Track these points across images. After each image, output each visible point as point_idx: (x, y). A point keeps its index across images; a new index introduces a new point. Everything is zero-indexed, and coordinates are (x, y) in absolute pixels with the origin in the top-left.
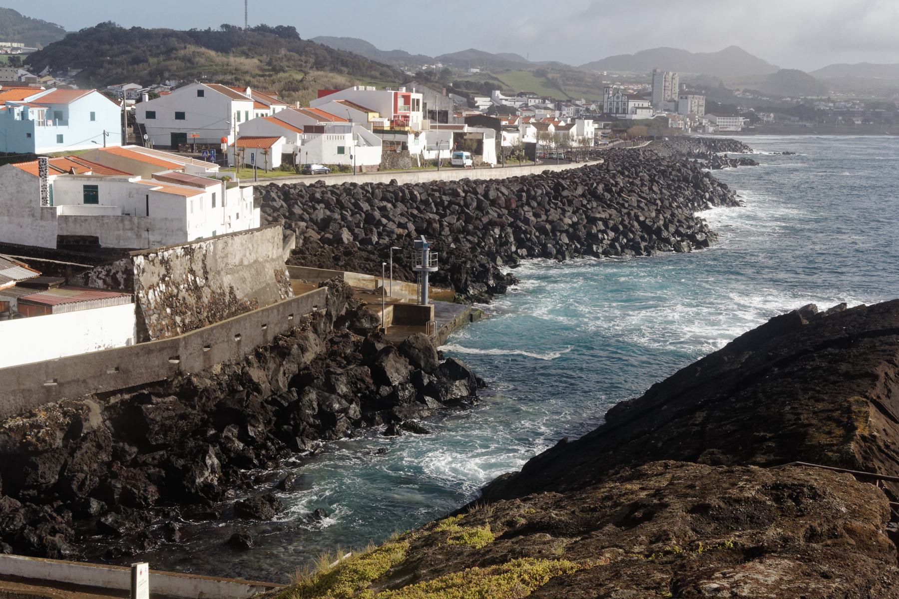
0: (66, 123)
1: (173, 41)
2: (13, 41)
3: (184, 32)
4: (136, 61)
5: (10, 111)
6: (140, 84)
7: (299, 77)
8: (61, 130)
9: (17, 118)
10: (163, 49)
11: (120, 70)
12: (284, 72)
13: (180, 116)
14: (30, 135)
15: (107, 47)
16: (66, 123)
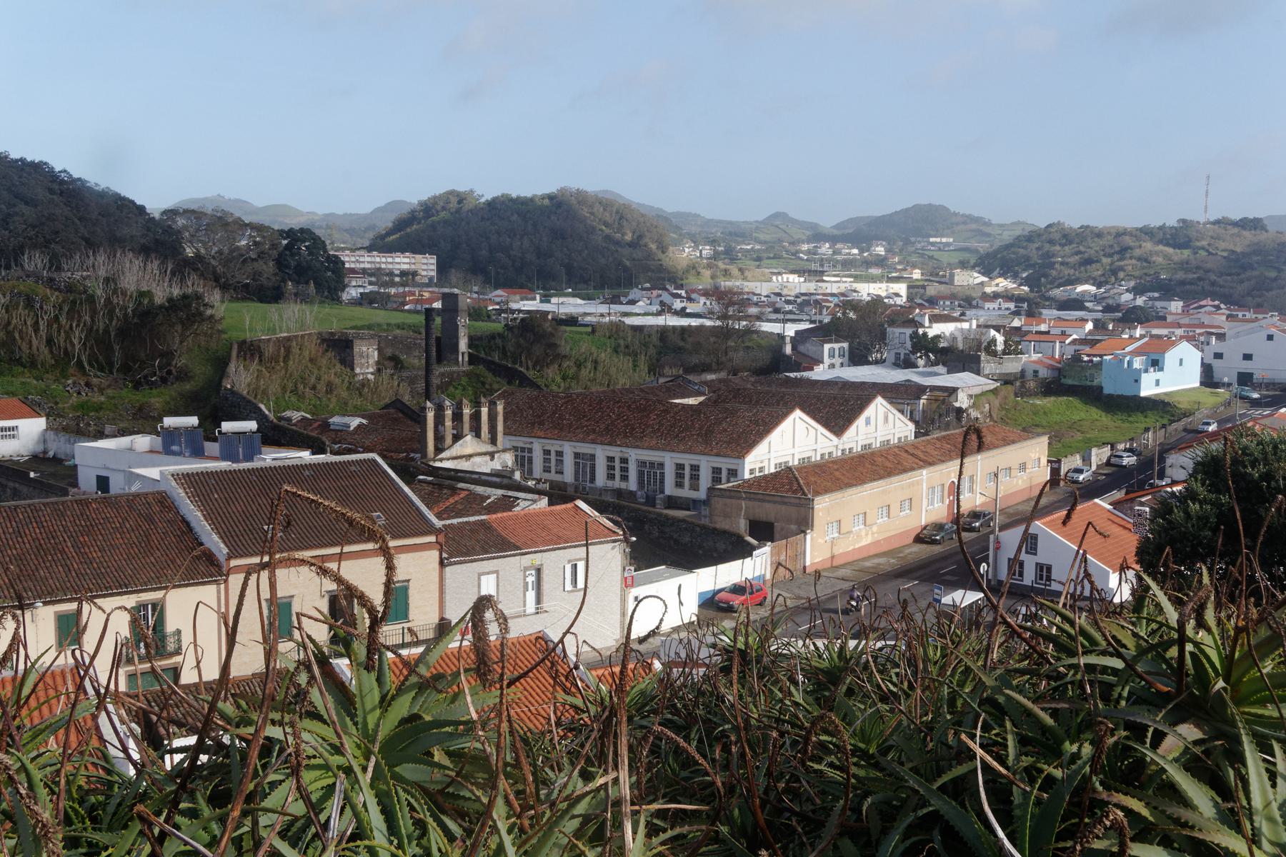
0: (1161, 369)
1: (1128, 240)
2: (942, 236)
3: (1137, 229)
4: (1089, 262)
5: (1122, 361)
7: (1273, 274)
8: (1159, 375)
10: (1117, 249)
12: (1253, 269)
13: (1248, 357)
14: (1137, 381)
15: (1058, 248)
16: (1161, 369)
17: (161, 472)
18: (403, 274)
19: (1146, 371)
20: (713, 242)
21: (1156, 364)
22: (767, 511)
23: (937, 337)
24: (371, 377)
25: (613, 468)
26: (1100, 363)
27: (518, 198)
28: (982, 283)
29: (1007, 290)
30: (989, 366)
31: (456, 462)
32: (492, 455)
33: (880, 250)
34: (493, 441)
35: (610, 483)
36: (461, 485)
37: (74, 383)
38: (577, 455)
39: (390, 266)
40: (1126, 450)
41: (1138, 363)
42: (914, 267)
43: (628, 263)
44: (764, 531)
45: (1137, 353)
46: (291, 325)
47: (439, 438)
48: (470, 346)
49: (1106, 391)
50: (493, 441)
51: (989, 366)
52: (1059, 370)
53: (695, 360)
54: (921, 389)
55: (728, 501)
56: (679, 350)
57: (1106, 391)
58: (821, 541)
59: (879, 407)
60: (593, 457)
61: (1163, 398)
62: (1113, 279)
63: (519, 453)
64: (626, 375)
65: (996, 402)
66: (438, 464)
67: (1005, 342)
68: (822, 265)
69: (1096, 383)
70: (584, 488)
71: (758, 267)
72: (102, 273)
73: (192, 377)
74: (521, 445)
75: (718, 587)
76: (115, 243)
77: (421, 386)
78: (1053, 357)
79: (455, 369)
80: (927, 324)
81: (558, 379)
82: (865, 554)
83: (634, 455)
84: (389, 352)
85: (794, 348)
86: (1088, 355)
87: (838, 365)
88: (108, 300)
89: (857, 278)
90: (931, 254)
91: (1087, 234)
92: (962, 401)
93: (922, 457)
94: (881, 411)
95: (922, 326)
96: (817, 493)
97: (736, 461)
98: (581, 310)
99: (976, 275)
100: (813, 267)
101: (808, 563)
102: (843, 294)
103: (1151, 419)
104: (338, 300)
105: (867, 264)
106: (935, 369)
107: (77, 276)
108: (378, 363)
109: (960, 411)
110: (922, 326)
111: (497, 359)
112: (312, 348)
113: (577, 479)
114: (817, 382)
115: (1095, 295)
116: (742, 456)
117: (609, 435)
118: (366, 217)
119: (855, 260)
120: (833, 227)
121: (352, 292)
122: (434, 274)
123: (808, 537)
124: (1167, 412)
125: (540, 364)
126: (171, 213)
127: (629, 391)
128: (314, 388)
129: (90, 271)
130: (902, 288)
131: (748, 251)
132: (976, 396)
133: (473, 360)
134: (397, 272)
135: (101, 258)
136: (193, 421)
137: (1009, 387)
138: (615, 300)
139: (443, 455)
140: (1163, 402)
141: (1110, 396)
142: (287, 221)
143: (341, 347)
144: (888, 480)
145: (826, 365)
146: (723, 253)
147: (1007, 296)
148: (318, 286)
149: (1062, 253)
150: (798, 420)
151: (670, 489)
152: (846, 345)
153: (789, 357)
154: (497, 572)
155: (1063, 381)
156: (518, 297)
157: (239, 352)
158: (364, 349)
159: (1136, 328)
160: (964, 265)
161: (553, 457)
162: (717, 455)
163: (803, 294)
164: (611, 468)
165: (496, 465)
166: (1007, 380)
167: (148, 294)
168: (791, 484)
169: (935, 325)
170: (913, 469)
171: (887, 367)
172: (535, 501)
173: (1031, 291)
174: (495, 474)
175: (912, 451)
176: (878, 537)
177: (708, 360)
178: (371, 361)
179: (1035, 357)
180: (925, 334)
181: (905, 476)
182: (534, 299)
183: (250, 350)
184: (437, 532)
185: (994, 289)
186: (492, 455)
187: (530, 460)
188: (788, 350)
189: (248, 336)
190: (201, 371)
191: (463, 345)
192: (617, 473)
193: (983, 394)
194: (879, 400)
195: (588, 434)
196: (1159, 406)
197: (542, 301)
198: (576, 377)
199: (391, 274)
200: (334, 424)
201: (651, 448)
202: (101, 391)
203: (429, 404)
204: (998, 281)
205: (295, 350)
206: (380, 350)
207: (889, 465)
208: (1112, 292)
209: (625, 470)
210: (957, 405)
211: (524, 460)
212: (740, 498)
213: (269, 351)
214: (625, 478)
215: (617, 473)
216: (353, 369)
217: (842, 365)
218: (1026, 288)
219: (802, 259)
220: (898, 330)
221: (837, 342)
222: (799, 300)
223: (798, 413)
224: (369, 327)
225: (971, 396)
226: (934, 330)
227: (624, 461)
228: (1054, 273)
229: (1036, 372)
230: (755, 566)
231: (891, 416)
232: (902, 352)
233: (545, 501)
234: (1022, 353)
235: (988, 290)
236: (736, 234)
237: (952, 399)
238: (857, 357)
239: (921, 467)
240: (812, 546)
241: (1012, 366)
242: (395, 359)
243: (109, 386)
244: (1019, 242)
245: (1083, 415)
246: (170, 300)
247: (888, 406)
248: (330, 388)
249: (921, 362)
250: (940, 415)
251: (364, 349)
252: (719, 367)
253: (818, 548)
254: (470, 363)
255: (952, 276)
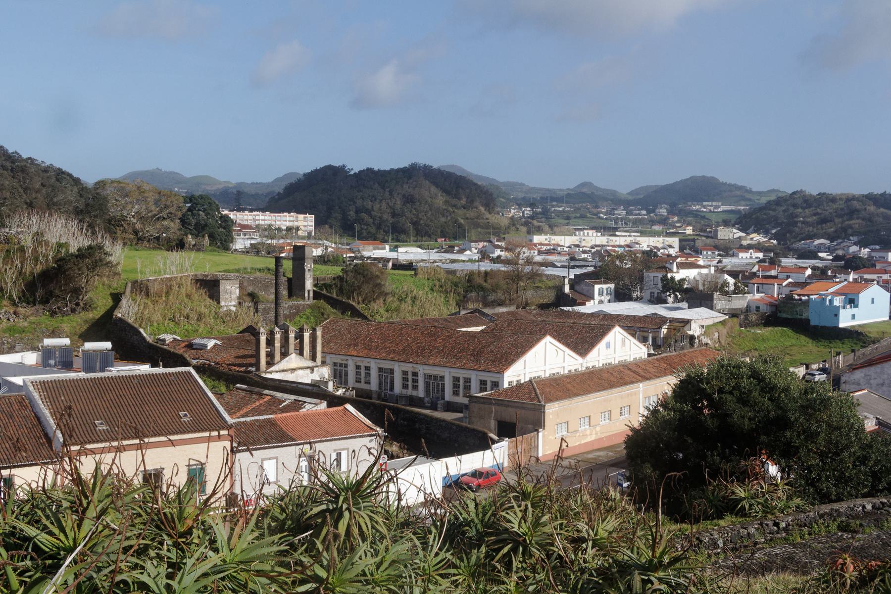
0: (857, 306)
3: (863, 196)
4: (824, 221)
5: (824, 300)
6: (828, 239)
9: (828, 303)
11: (811, 229)
14: (837, 315)
15: (800, 210)
16: (857, 306)
17: (24, 381)
18: (289, 229)
19: (844, 308)
20: (532, 205)
21: (852, 302)
22: (509, 415)
23: (683, 280)
24: (234, 309)
25: (407, 380)
26: (807, 302)
27: (379, 170)
28: (740, 238)
29: (759, 243)
30: (720, 302)
31: (283, 374)
32: (312, 369)
33: (663, 212)
34: (313, 358)
35: (404, 391)
36: (266, 392)
37: (6, 312)
38: (380, 370)
39: (278, 223)
40: (819, 370)
41: (838, 301)
42: (689, 224)
43: (462, 221)
44: (507, 430)
45: (837, 293)
46: (174, 269)
47: (270, 355)
48: (315, 285)
49: (812, 323)
50: (313, 358)
51: (720, 302)
52: (776, 306)
53: (491, 297)
54: (663, 320)
55: (482, 406)
56: (481, 288)
57: (812, 323)
58: (551, 437)
59: (617, 334)
60: (392, 371)
61: (856, 328)
62: (843, 235)
63: (338, 368)
64: (438, 308)
65: (724, 331)
66: (268, 376)
67: (735, 284)
68: (616, 223)
69: (804, 317)
70: (385, 395)
71: (568, 224)
72: (35, 229)
73: (96, 308)
74: (339, 361)
75: (462, 472)
76: (51, 206)
77: (272, 316)
78: (772, 296)
79: (301, 302)
80: (675, 269)
81: (382, 311)
82: (596, 447)
83: (422, 370)
84: (250, 289)
85: (572, 288)
86: (799, 295)
87: (606, 301)
88: (35, 250)
89: (643, 234)
90: (702, 214)
91: (824, 199)
92: (695, 330)
93: (642, 373)
94: (619, 338)
95: (671, 271)
96: (550, 400)
97: (498, 375)
98: (419, 257)
99: (735, 231)
100: (609, 224)
101: (540, 455)
102: (628, 246)
103: (848, 345)
104: (227, 249)
105: (653, 222)
106: (680, 305)
107: (13, 231)
108: (239, 298)
109: (692, 338)
110: (671, 271)
111: (334, 296)
112: (189, 287)
113: (380, 387)
114: (584, 314)
115: (829, 248)
116: (501, 372)
117: (405, 354)
118: (268, 185)
119: (644, 219)
120: (628, 194)
121: (241, 243)
122: (312, 228)
123: (540, 434)
124: (859, 340)
125: (367, 300)
126: (101, 184)
127: (437, 320)
128: (187, 317)
129: (25, 228)
130: (675, 241)
131: (560, 212)
132: (708, 326)
133: (317, 296)
134: (284, 228)
135: (35, 219)
136: (108, 345)
137: (735, 319)
138: (450, 249)
139: (273, 369)
140: (857, 332)
141: (815, 327)
142: (208, 188)
143: (210, 286)
144: (609, 391)
145: (596, 301)
146: (540, 213)
147: (758, 247)
148: (212, 237)
149: (804, 215)
150: (548, 345)
151: (448, 396)
152: (612, 286)
153: (567, 295)
154: (276, 458)
155: (779, 314)
156: (371, 247)
157: (132, 290)
158: (228, 287)
159: (850, 273)
160: (726, 223)
161: (363, 371)
162: (484, 371)
163: (597, 246)
164: (405, 379)
165: (316, 376)
166: (733, 314)
167: (66, 245)
168: (530, 393)
169: (681, 271)
170: (632, 382)
171: (644, 303)
172: (316, 404)
173: (779, 244)
174: (314, 384)
175: (633, 369)
176: (600, 436)
177: (502, 298)
178: (234, 297)
179: (758, 296)
180: (673, 278)
181: (624, 388)
182: (384, 249)
183: (141, 288)
184: (229, 427)
185: (749, 242)
186: (312, 369)
187: (346, 375)
188: (567, 289)
189: (139, 277)
190: (103, 303)
191: (309, 284)
192: (410, 383)
193: (714, 325)
194: (617, 329)
195: (389, 354)
196: (855, 336)
197: (391, 250)
198: (397, 310)
199: (279, 229)
200: (196, 344)
201: (435, 365)
202: (25, 317)
203: (277, 329)
204: (752, 236)
205: (175, 288)
206: (241, 287)
207: (612, 379)
208: (842, 245)
209: (415, 381)
210: (690, 333)
211: (339, 376)
212: (491, 404)
213: (154, 288)
214: (415, 387)
215: (410, 383)
216: (219, 302)
217: (609, 301)
218: (775, 242)
219: (602, 218)
220: (652, 275)
221: (605, 283)
222: (593, 250)
223: (548, 339)
224: (238, 271)
225: (703, 326)
226: (679, 275)
227: (415, 374)
228: (797, 229)
229: (758, 308)
230: (496, 456)
231: (627, 342)
232: (656, 291)
233: (325, 404)
234: (748, 293)
235: (744, 243)
236: (553, 199)
237: (686, 328)
238: (621, 295)
239: (639, 381)
240: (544, 441)
241: (740, 302)
242: (253, 296)
243: (32, 314)
244: (769, 205)
245: (794, 341)
246: (79, 250)
247: (625, 334)
248: (200, 317)
249: (670, 299)
250: (676, 341)
251: (228, 287)
252: (511, 301)
253: (546, 444)
254: (314, 299)
255: (716, 232)
